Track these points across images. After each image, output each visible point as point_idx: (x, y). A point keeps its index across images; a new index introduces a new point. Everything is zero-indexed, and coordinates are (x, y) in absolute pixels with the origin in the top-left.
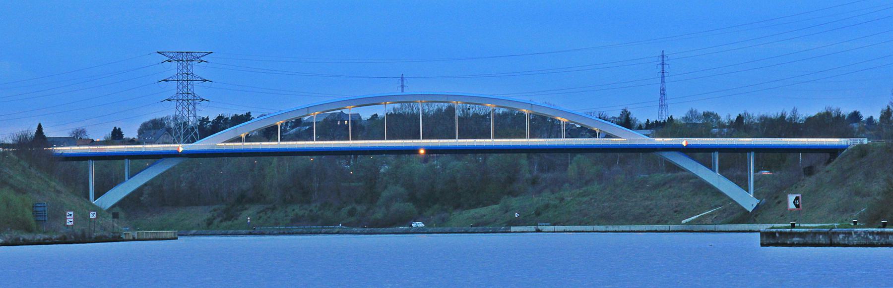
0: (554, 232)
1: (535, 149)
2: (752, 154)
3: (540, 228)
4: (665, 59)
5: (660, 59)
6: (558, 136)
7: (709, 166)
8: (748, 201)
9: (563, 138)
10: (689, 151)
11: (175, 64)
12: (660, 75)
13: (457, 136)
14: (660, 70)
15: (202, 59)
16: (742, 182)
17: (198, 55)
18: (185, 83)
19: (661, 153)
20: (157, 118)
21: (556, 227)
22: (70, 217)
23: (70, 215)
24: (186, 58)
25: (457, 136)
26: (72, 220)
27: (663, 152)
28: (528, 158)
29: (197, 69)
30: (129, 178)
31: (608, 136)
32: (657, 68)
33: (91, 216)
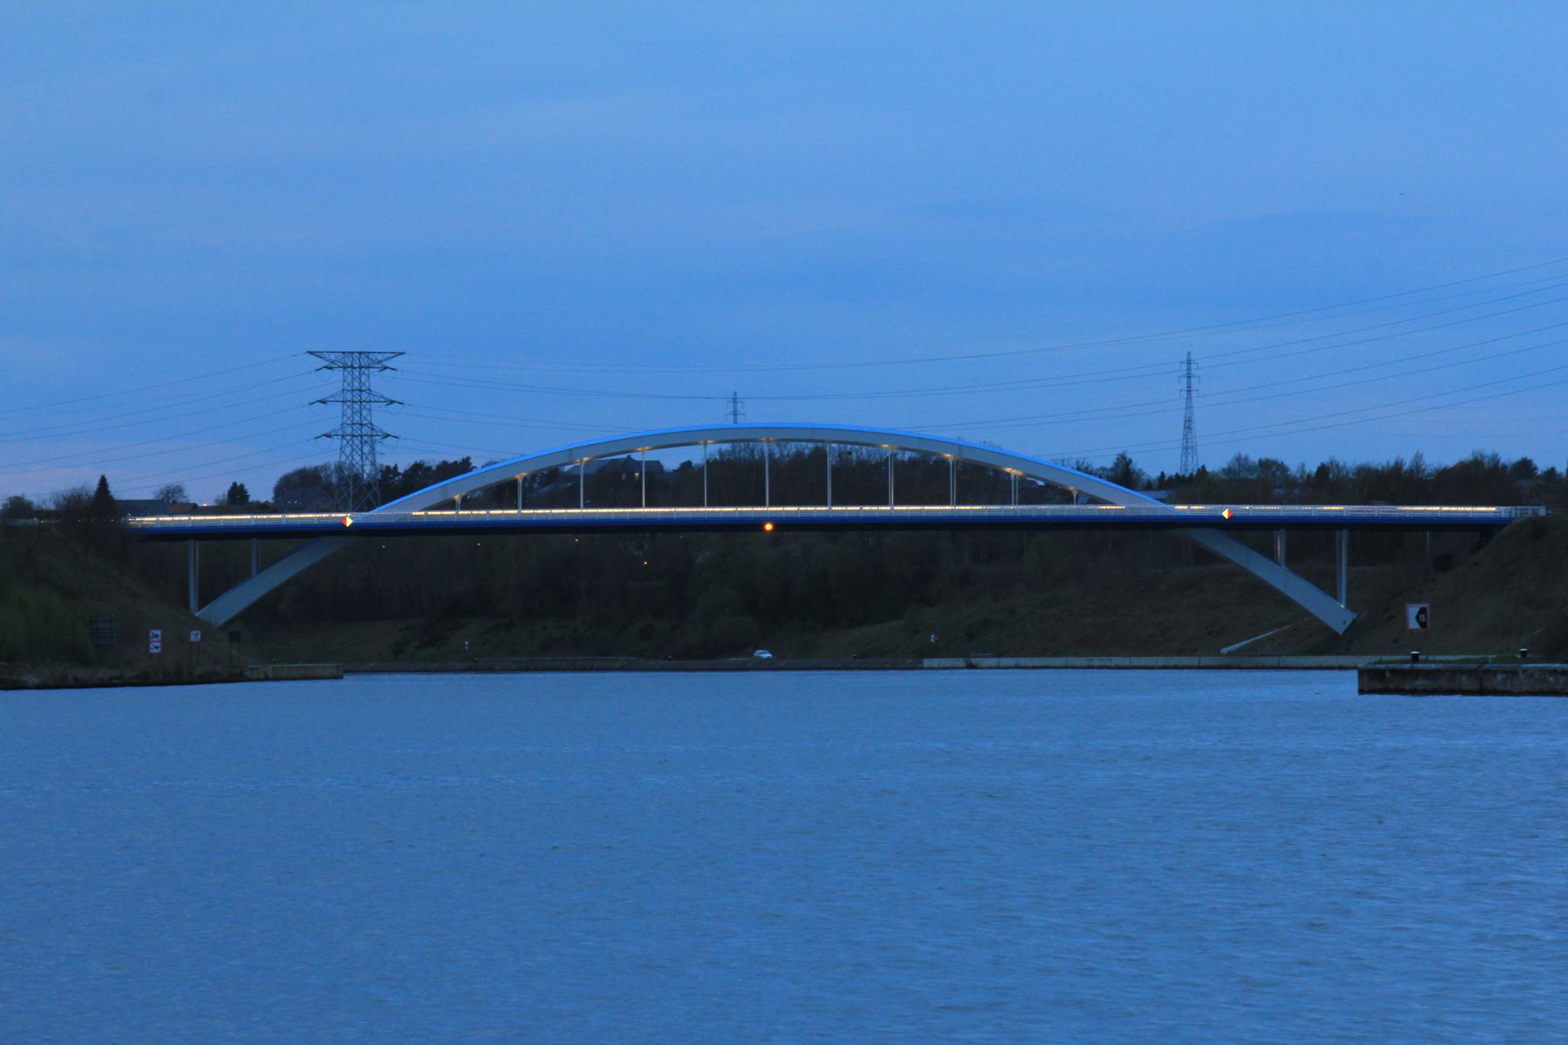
2: (1345, 533)
3: (974, 661)
4: (1193, 366)
8: (1335, 613)
12: (1184, 394)
14: (1184, 386)
15: (387, 363)
16: (1327, 584)
17: (380, 357)
22: (155, 639)
24: (357, 363)
29: (377, 382)
30: (259, 572)
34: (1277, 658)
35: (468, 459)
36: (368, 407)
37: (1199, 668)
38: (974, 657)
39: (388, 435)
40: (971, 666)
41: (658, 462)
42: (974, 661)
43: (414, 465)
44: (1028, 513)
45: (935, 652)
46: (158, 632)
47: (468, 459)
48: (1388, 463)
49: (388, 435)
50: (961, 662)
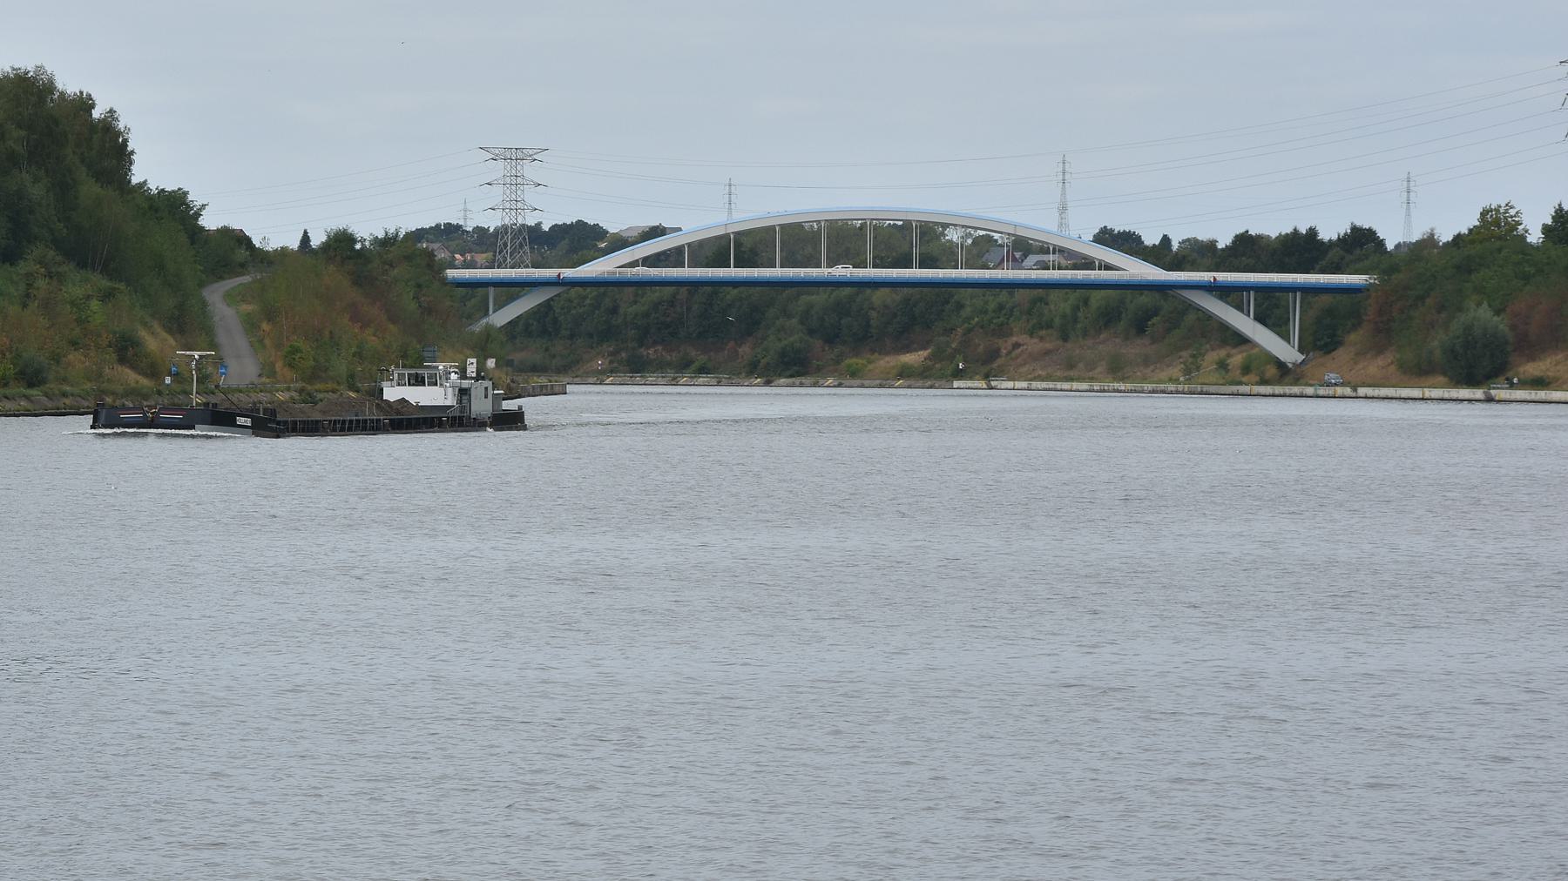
0: (1071, 391)
1: (465, 283)
2: (1298, 294)
3: (993, 383)
4: (1412, 184)
5: (1405, 183)
6: (908, 265)
7: (1239, 307)
8: (1288, 352)
9: (962, 268)
10: (1224, 292)
11: (501, 163)
12: (1405, 205)
13: (732, 265)
14: (1405, 200)
15: (535, 157)
16: (1283, 332)
17: (531, 152)
18: (513, 188)
19: (1179, 292)
20: (1342, 234)
21: (1016, 383)
22: (471, 366)
23: (472, 363)
24: (516, 156)
25: (732, 265)
26: (475, 370)
27: (1184, 291)
28: (1010, 293)
29: (529, 171)
30: (494, 312)
31: (1108, 267)
32: (1400, 196)
33: (493, 365)
34: (1012, 383)
35: (541, 223)
36: (522, 188)
37: (1273, 396)
38: (1494, 388)
39: (536, 209)
40: (1490, 400)
41: (1236, 236)
42: (993, 383)
43: (1242, 235)
44: (1334, 281)
45: (959, 374)
46: (474, 360)
47: (541, 223)
48: (306, 239)
49: (536, 209)
50: (1479, 393)
